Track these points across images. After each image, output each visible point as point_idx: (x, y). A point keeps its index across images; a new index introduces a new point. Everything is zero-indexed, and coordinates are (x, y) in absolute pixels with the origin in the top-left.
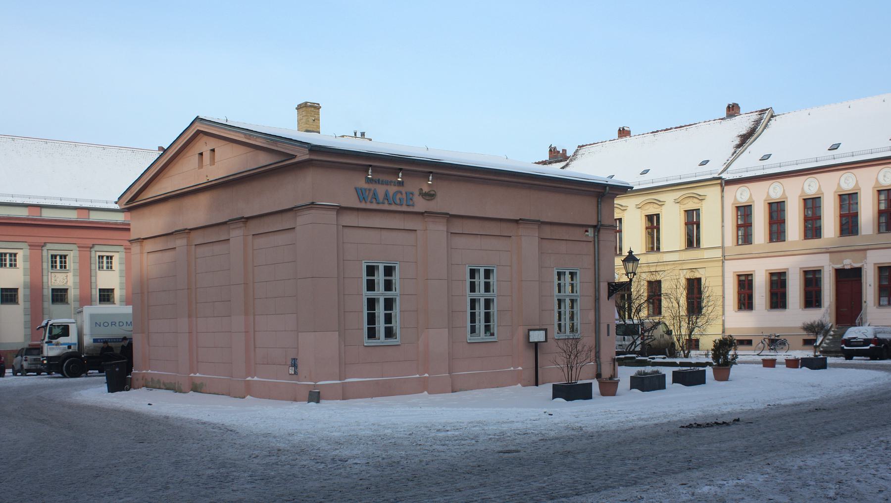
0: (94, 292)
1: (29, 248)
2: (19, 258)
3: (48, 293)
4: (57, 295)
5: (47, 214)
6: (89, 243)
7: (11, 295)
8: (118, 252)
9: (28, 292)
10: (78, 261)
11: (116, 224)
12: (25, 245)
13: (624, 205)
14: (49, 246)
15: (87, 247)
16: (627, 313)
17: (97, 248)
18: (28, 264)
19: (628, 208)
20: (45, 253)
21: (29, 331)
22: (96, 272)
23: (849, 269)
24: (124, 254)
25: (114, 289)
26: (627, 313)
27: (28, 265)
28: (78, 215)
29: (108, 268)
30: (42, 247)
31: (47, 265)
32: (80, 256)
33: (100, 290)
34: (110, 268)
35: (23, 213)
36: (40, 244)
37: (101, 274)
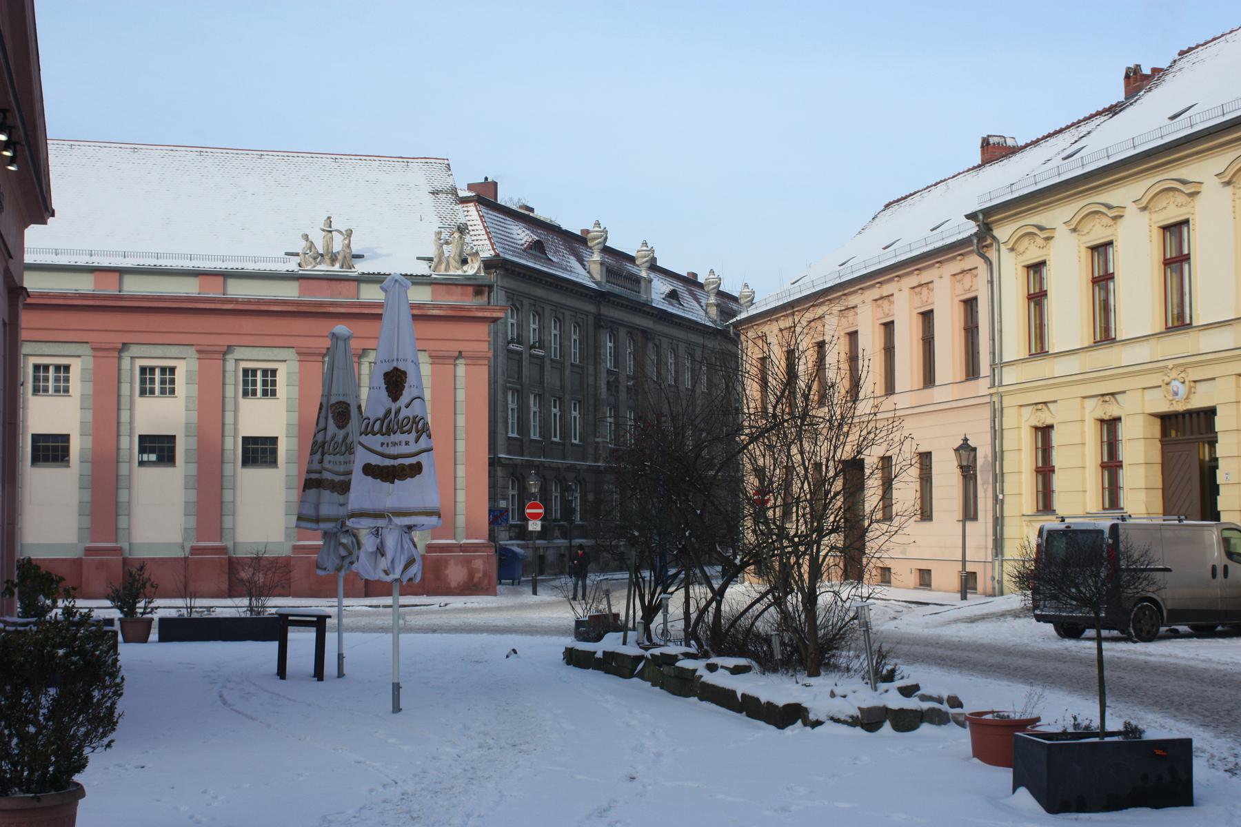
0: (124, 442)
1: (197, 356)
2: (180, 376)
3: (234, 448)
4: (255, 451)
5: (239, 290)
6: (118, 339)
7: (55, 449)
8: (285, 361)
9: (193, 443)
10: (297, 383)
11: (64, 296)
12: (86, 350)
13: (1191, 180)
14: (239, 353)
15: (319, 354)
16: (815, 551)
17: (134, 350)
18: (90, 386)
19: (1204, 189)
20: (230, 365)
21: (87, 522)
22: (236, 404)
23: (23, 258)
24: (91, 359)
25: (277, 438)
26: (815, 551)
27: (90, 388)
28: (95, 284)
29: (57, 390)
30: (455, 360)
31: (233, 387)
32: (301, 372)
33: (246, 440)
34: (270, 392)
35: (85, 284)
36: (317, 351)
37: (246, 405)
